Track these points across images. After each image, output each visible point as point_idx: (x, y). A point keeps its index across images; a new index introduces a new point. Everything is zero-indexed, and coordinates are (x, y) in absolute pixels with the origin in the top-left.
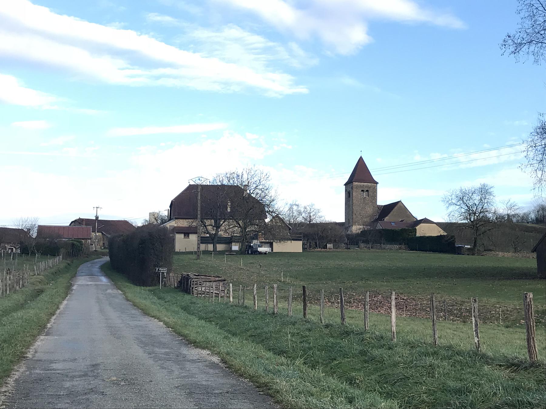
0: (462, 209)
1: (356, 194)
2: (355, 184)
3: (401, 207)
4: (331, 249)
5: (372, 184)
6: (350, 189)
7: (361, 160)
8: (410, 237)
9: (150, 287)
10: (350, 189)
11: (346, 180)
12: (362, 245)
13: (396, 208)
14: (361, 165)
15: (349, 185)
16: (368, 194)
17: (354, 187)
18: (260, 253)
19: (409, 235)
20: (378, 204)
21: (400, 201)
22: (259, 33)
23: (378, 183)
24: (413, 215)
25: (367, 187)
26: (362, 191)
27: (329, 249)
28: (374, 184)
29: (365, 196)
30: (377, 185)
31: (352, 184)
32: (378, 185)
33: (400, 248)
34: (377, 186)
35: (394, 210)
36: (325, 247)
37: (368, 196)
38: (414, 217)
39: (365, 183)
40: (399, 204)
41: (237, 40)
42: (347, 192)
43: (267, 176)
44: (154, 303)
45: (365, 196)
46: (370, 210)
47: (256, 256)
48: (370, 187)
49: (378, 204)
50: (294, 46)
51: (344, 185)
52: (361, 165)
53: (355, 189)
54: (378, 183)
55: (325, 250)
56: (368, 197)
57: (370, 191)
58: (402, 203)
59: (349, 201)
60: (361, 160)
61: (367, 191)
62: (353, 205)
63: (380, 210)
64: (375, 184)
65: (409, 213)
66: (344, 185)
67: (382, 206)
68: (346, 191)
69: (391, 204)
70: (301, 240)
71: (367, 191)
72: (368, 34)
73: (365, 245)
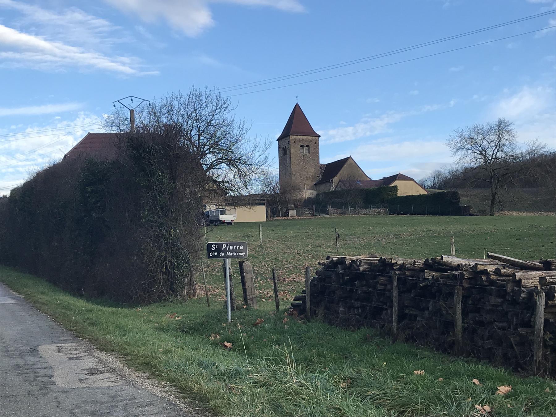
0: (476, 153)
1: (295, 151)
2: (293, 137)
3: (351, 164)
4: (295, 217)
5: (313, 137)
6: (286, 145)
7: (297, 108)
8: (390, 197)
9: (483, 269)
10: (286, 145)
11: (278, 135)
12: (331, 210)
13: (347, 163)
14: (297, 113)
15: (284, 139)
16: (309, 150)
17: (292, 141)
18: (223, 223)
19: (389, 195)
20: (320, 163)
21: (350, 157)
22: (104, 17)
23: (320, 136)
24: (366, 174)
25: (306, 141)
26: (302, 146)
27: (291, 217)
28: (315, 137)
29: (305, 153)
30: (318, 138)
31: (288, 137)
32: (320, 139)
33: (379, 213)
34: (318, 140)
35: (343, 169)
36: (286, 214)
37: (309, 153)
38: (367, 177)
39: (304, 137)
40: (348, 162)
41: (81, 23)
42: (281, 149)
43: (226, 105)
44: (126, 316)
45: (305, 153)
46: (312, 171)
47: (216, 229)
48: (311, 141)
49: (320, 163)
50: (141, 29)
51: (277, 140)
52: (297, 113)
53: (292, 145)
54: (320, 136)
55: (285, 218)
56: (308, 154)
57: (310, 146)
58: (353, 160)
59: (285, 159)
60: (297, 108)
61: (307, 146)
62: (290, 164)
63: (323, 169)
64: (317, 138)
65: (361, 171)
66: (277, 140)
67: (325, 165)
68: (279, 148)
69: (336, 161)
70: (263, 204)
71: (307, 146)
72: (213, 18)
73: (336, 211)
